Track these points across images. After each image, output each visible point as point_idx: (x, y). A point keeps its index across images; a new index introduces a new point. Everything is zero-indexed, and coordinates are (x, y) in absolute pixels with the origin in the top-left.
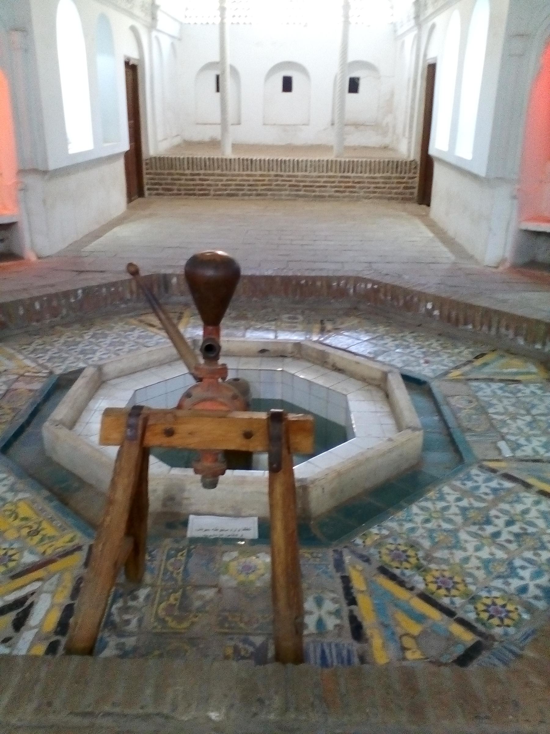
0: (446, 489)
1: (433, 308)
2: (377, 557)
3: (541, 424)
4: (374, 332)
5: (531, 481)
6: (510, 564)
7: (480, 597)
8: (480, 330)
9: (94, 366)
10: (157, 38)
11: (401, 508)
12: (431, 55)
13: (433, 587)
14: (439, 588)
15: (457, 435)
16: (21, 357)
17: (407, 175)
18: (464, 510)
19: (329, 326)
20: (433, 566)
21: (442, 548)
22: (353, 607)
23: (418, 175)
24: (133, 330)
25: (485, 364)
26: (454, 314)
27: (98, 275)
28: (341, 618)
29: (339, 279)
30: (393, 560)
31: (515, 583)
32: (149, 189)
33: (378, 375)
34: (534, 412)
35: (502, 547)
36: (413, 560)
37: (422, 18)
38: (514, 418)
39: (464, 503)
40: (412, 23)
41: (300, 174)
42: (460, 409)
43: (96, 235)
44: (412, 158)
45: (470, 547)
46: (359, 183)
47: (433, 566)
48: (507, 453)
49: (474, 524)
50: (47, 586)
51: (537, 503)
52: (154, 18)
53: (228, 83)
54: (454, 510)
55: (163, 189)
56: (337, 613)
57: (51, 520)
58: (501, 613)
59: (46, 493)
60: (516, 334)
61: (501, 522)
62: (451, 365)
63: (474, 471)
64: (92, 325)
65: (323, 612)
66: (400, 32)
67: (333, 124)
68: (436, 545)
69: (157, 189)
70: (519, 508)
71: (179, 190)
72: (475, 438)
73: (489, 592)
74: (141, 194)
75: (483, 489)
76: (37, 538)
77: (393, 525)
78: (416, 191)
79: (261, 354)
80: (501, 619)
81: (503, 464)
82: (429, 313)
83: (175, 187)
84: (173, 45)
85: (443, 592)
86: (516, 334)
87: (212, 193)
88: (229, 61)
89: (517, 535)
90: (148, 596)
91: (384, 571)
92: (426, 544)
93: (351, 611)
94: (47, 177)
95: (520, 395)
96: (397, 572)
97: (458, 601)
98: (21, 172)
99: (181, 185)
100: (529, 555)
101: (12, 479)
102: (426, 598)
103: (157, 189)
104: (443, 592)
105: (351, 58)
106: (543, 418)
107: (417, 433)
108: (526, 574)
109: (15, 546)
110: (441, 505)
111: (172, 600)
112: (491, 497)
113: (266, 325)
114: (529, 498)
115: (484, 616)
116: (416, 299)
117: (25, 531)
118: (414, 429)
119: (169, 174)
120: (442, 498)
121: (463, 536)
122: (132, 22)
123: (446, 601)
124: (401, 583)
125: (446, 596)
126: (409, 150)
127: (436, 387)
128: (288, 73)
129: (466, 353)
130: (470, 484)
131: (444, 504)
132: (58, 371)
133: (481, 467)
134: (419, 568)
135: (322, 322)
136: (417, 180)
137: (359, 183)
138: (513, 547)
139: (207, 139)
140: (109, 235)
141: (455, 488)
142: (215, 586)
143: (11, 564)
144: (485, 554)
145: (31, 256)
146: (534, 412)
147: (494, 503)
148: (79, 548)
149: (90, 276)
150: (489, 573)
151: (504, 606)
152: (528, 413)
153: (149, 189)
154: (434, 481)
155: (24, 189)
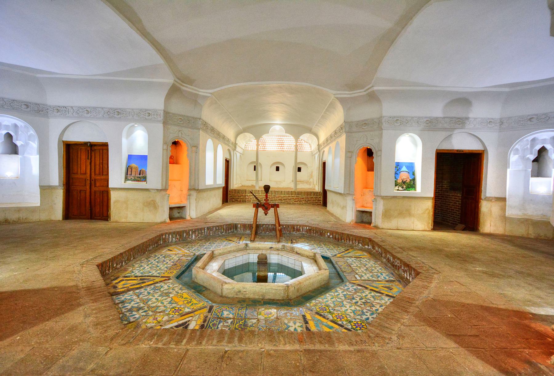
0: (338, 289)
1: (330, 235)
2: (315, 309)
3: (369, 270)
4: (310, 243)
5: (367, 286)
6: (362, 311)
7: (352, 321)
8: (347, 242)
9: (211, 251)
10: (236, 153)
11: (323, 295)
12: (324, 160)
13: (335, 318)
14: (337, 318)
15: (340, 273)
16: (184, 250)
17: (318, 197)
18: (345, 295)
19: (294, 241)
20: (335, 312)
21: (338, 307)
22: (307, 325)
23: (322, 197)
24: (224, 242)
25: (349, 253)
26: (337, 236)
27: (212, 224)
28: (303, 328)
29: (297, 225)
30: (321, 310)
31: (364, 317)
32: (229, 200)
33: (312, 255)
34: (367, 266)
35: (359, 306)
36: (328, 310)
37: (320, 149)
38: (360, 268)
39: (345, 293)
40: (317, 151)
41: (282, 195)
42: (341, 266)
43: (211, 212)
44: (320, 191)
45: (348, 306)
46: (302, 199)
47: (335, 312)
48: (358, 278)
49: (348, 299)
50: (194, 319)
51: (370, 293)
52: (235, 147)
53: (259, 168)
54: (341, 295)
55: (235, 200)
56: (301, 326)
57: (196, 298)
58: (360, 326)
59: (193, 290)
60: (359, 243)
61: (358, 299)
62: (338, 253)
63: (348, 284)
64: (209, 240)
65: (296, 326)
66: (314, 154)
67: (293, 181)
68: (335, 306)
69: (233, 200)
70: (364, 294)
71: (241, 200)
72: (347, 274)
73: (355, 320)
74: (227, 201)
75: (351, 289)
76: (190, 304)
77: (320, 300)
78: (322, 202)
79: (270, 249)
80: (361, 328)
81: (357, 282)
82: (329, 237)
83: (239, 199)
84: (240, 155)
85: (339, 320)
86: (359, 243)
87: (252, 201)
88: (259, 161)
89: (364, 303)
90: (232, 322)
91: (317, 313)
92: (332, 305)
93: (306, 326)
94: (198, 191)
95: (361, 261)
96: (322, 314)
97: (345, 323)
98: (190, 190)
99: (241, 199)
100: (369, 308)
101: (181, 286)
102: (333, 321)
103: (233, 200)
104: (339, 320)
105: (298, 161)
106: (370, 268)
107: (327, 271)
108: (368, 314)
109: (182, 306)
110: (336, 294)
111: (241, 323)
112: (354, 291)
113: (272, 241)
114: (367, 292)
115: (355, 327)
116: (324, 232)
117: (186, 302)
118: (326, 270)
119: (237, 195)
120: (337, 292)
121: (345, 303)
122: (229, 148)
123: (340, 323)
124: (324, 317)
125: (340, 321)
126: (318, 189)
127: (334, 260)
128: (278, 166)
129: (343, 250)
130: (346, 288)
131: (337, 293)
132: (197, 254)
133: (350, 283)
134: (330, 312)
135: (292, 240)
136: (322, 198)
137: (302, 199)
138: (363, 306)
139: (250, 185)
140: (215, 213)
141: (341, 289)
142: (257, 319)
143: (180, 312)
144: (353, 308)
145: (188, 218)
146: (367, 266)
147: (355, 293)
148: (205, 307)
149: (209, 224)
150: (355, 314)
151: (361, 324)
152: (365, 266)
153: (229, 200)
154: (333, 287)
155: (190, 195)
